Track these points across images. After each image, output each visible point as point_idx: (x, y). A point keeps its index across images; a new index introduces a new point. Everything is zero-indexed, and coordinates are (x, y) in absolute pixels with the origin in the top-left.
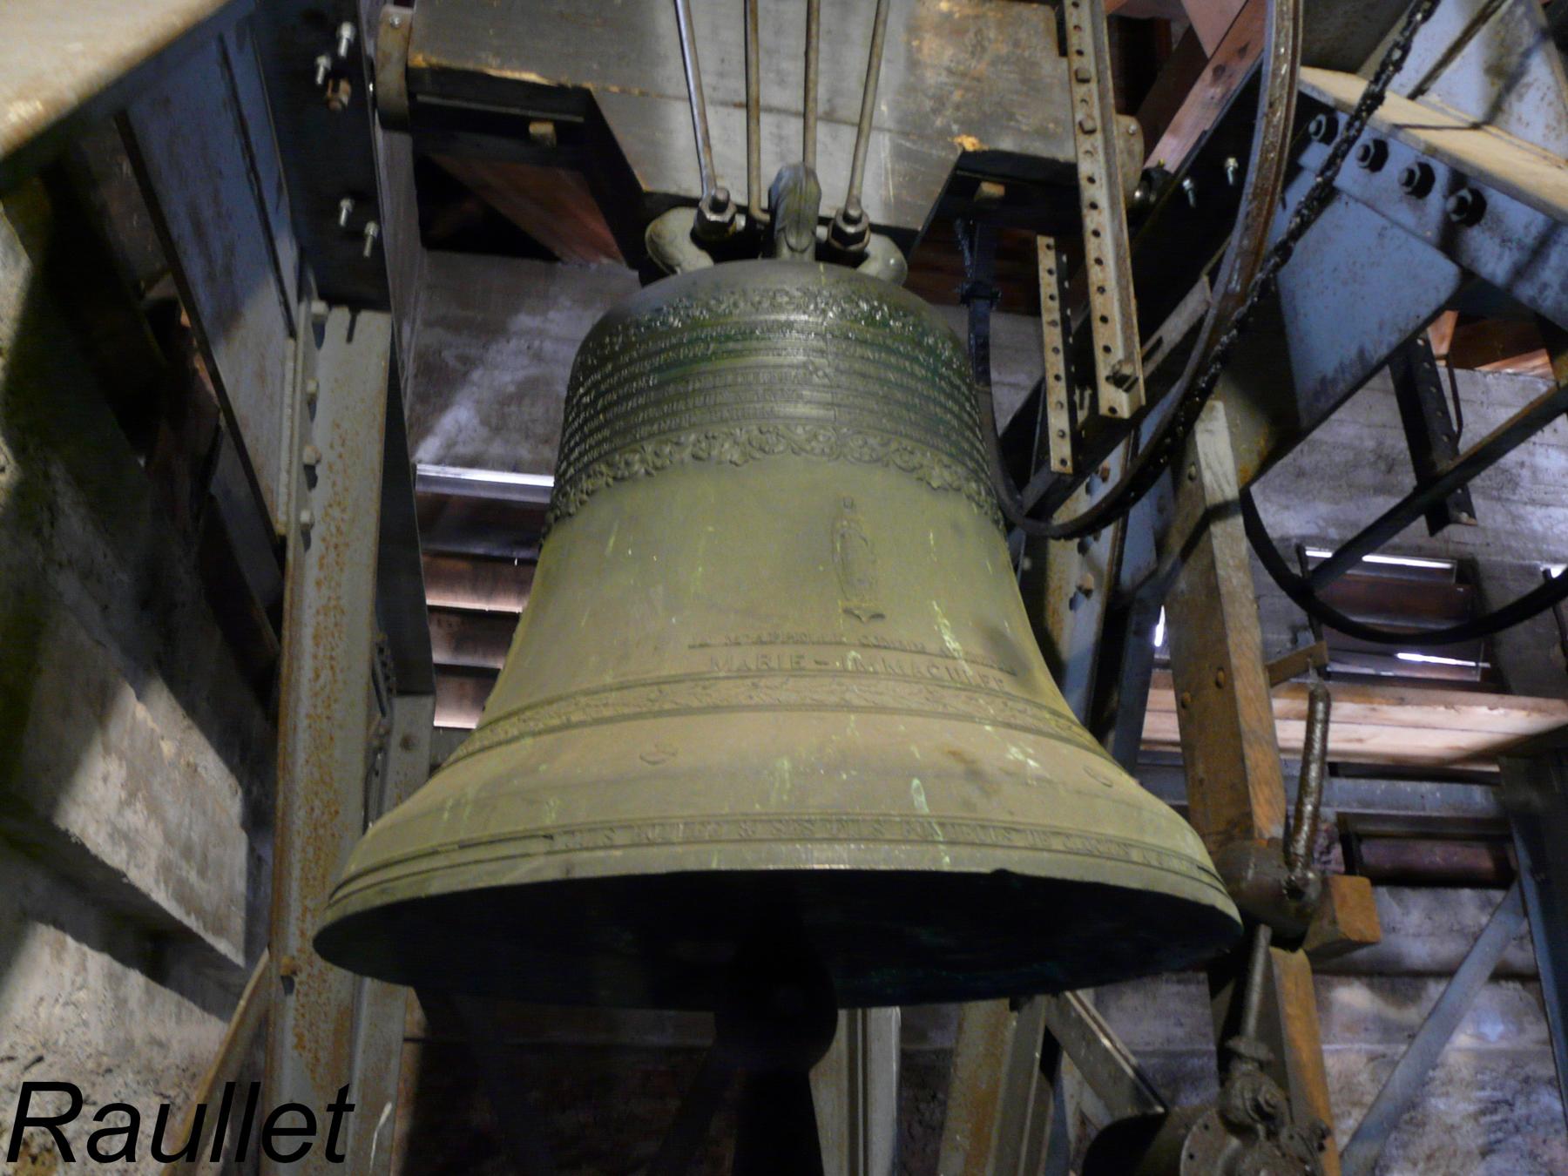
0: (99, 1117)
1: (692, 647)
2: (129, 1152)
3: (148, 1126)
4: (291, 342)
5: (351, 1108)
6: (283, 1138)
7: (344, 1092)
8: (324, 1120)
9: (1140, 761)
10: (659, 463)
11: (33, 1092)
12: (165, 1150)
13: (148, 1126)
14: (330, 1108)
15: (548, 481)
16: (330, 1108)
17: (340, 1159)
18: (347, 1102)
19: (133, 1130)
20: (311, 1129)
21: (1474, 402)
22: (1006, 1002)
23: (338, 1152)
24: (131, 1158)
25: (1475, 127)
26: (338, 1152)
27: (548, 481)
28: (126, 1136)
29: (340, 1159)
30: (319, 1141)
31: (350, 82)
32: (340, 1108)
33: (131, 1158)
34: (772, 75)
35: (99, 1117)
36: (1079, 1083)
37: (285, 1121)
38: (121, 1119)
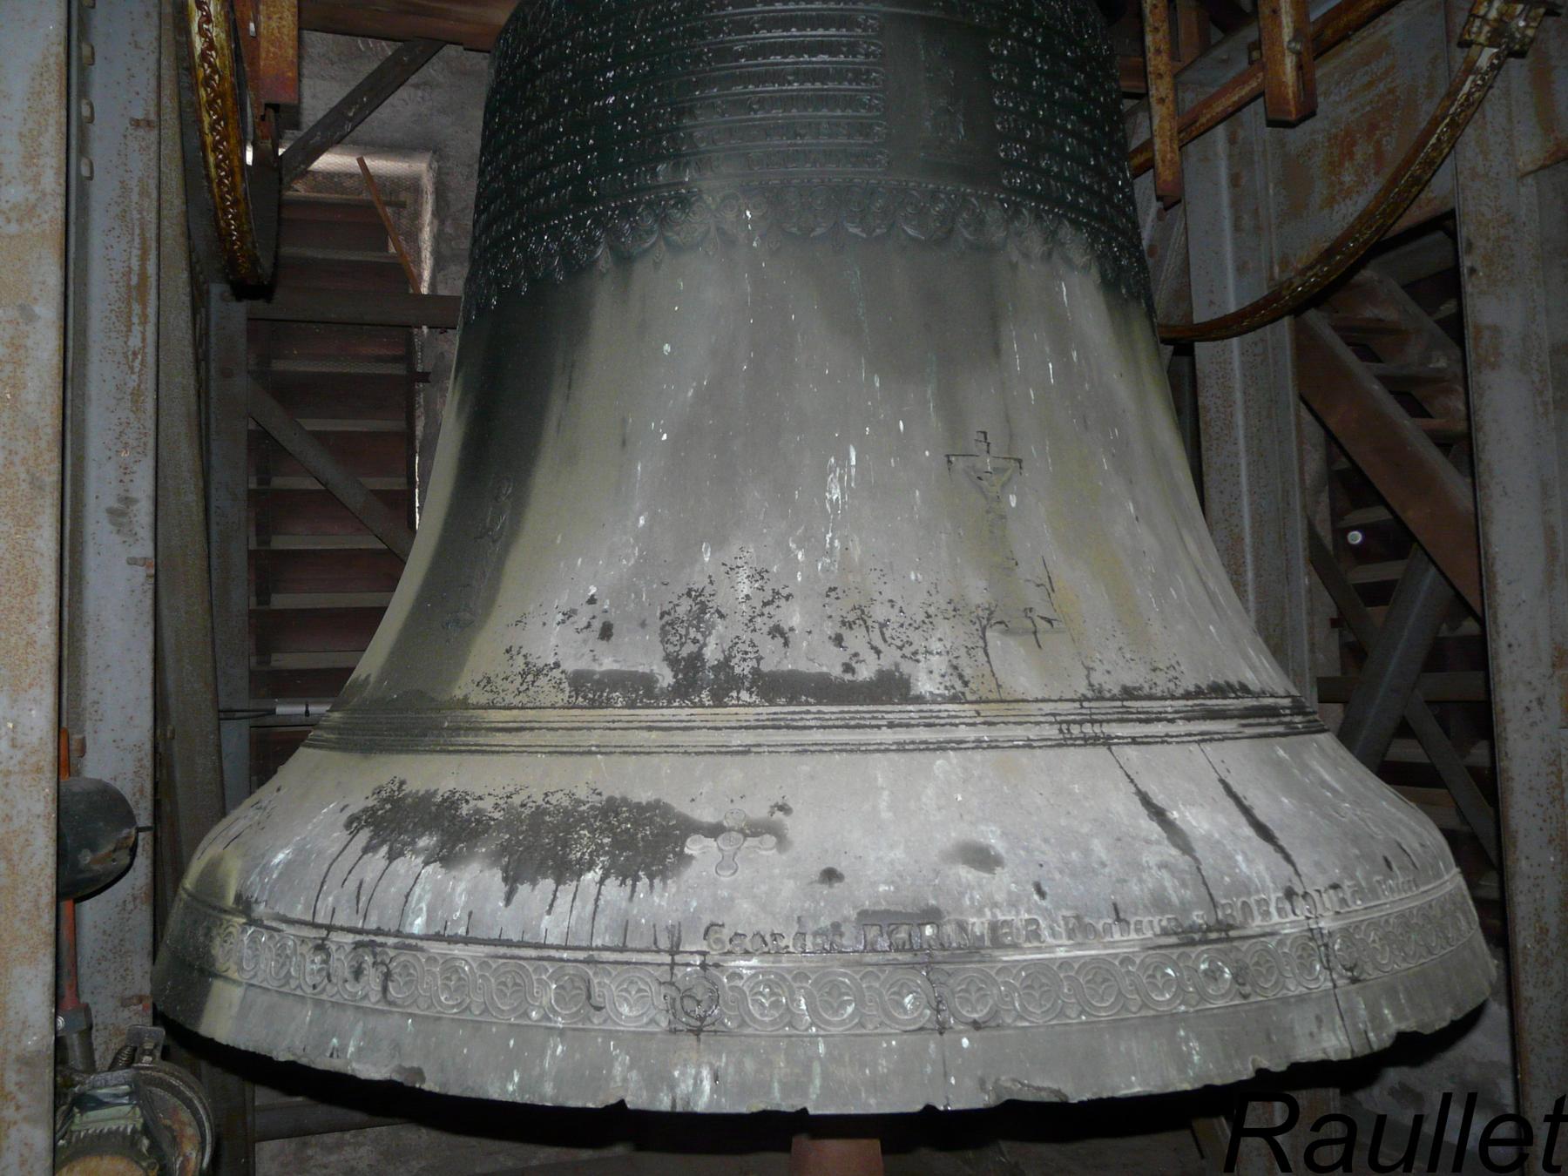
0: (1316, 1127)
1: (1115, 905)
2: (1346, 1162)
3: (1364, 1139)
4: (345, 836)
6: (1339, 1135)
9: (126, 1088)
11: (1196, 344)
12: (1383, 1161)
13: (1364, 1139)
14: (1547, 1118)
15: (424, 290)
17: (1557, 1169)
19: (1349, 1142)
22: (1551, 1113)
23: (1554, 1162)
24: (1348, 1169)
26: (1554, 1162)
27: (424, 290)
33: (1348, 1169)
35: (1316, 1127)
36: (1065, 1096)
38: (1336, 1130)
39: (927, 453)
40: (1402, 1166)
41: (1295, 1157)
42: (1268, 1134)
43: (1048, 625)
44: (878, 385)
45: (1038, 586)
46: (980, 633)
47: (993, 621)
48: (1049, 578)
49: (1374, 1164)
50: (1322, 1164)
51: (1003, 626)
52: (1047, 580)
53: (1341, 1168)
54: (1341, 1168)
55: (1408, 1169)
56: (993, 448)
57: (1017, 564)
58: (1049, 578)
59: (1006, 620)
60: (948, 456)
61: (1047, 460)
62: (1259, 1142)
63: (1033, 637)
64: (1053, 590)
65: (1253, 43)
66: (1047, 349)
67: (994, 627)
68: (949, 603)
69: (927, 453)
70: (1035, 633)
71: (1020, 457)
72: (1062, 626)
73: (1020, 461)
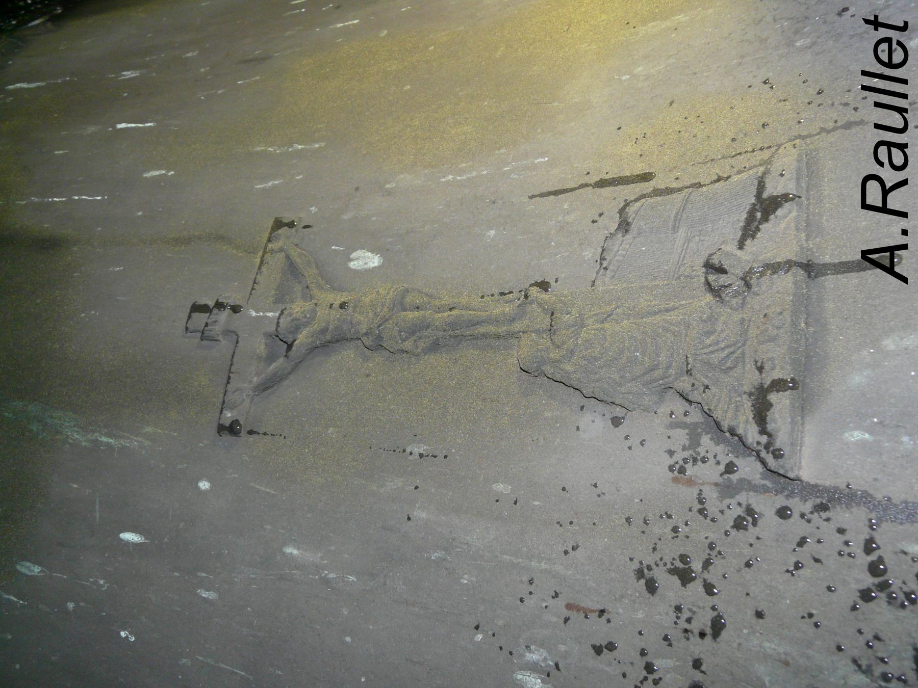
0: (881, 164)
2: (902, 147)
7: (867, 22)
8: (883, 33)
14: (876, 29)
17: (906, 23)
18: (872, 18)
19: (890, 145)
20: (889, 40)
23: (902, 25)
24: (906, 146)
26: (902, 25)
29: (906, 23)
32: (875, 23)
33: (906, 146)
35: (881, 164)
37: (884, 57)
39: (204, 485)
40: (904, 114)
41: (900, 176)
42: (885, 192)
43: (786, 215)
44: (37, 569)
45: (624, 226)
46: (798, 506)
47: (752, 435)
48: (602, 184)
49: (903, 131)
50: (903, 161)
51: (780, 401)
52: (607, 191)
53: (905, 150)
54: (905, 150)
55: (906, 111)
56: (231, 298)
57: (544, 286)
58: (602, 184)
59: (752, 378)
60: (221, 429)
61: (299, 154)
62: (890, 197)
63: (830, 281)
64: (646, 177)
65: (670, 414)
66: (91, 129)
67: (782, 440)
68: (651, 587)
69: (204, 485)
70: (811, 269)
71: (271, 222)
72: (787, 159)
73: (279, 224)
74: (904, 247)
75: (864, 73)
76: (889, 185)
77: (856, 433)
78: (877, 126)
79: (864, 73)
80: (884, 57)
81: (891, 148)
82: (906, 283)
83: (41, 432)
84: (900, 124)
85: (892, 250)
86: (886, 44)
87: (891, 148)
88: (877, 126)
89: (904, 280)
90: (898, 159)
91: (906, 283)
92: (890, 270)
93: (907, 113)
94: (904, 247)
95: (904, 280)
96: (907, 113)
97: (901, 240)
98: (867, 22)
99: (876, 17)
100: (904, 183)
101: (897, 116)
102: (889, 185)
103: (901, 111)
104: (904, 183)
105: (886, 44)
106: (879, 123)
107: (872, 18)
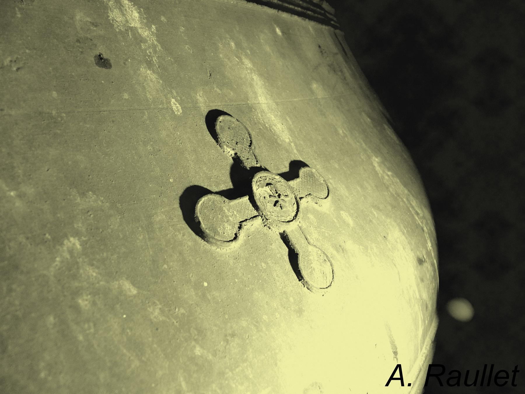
0: (450, 373)
2: (458, 384)
5: (518, 371)
7: (516, 367)
8: (511, 374)
10: (293, 193)
14: (513, 371)
16: (513, 371)
17: (516, 386)
18: (518, 370)
19: (459, 378)
20: (508, 377)
21: (268, 227)
23: (515, 384)
24: (459, 385)
25: (266, 170)
26: (515, 384)
28: (394, 377)
29: (516, 386)
30: (510, 380)
31: (332, 21)
32: (515, 371)
34: (153, 80)
35: (450, 373)
37: (501, 375)
38: (456, 374)
53: (457, 385)
54: (457, 385)
55: (475, 385)
74: (403, 385)
75: (492, 366)
76: (440, 377)
77: (174, 107)
78: (468, 372)
79: (492, 366)
80: (501, 375)
81: (393, 377)
82: (386, 386)
83: (239, 268)
84: (469, 383)
85: (401, 379)
86: (506, 376)
87: (393, 377)
88: (468, 372)
89: (387, 385)
90: (452, 382)
91: (386, 386)
92: (392, 378)
93: (474, 386)
94: (403, 385)
95: (387, 385)
96: (474, 386)
97: (406, 383)
98: (516, 367)
99: (518, 371)
100: (441, 385)
101: (473, 382)
102: (440, 377)
103: (475, 383)
104: (441, 385)
105: (506, 376)
106: (480, 372)
107: (518, 370)
